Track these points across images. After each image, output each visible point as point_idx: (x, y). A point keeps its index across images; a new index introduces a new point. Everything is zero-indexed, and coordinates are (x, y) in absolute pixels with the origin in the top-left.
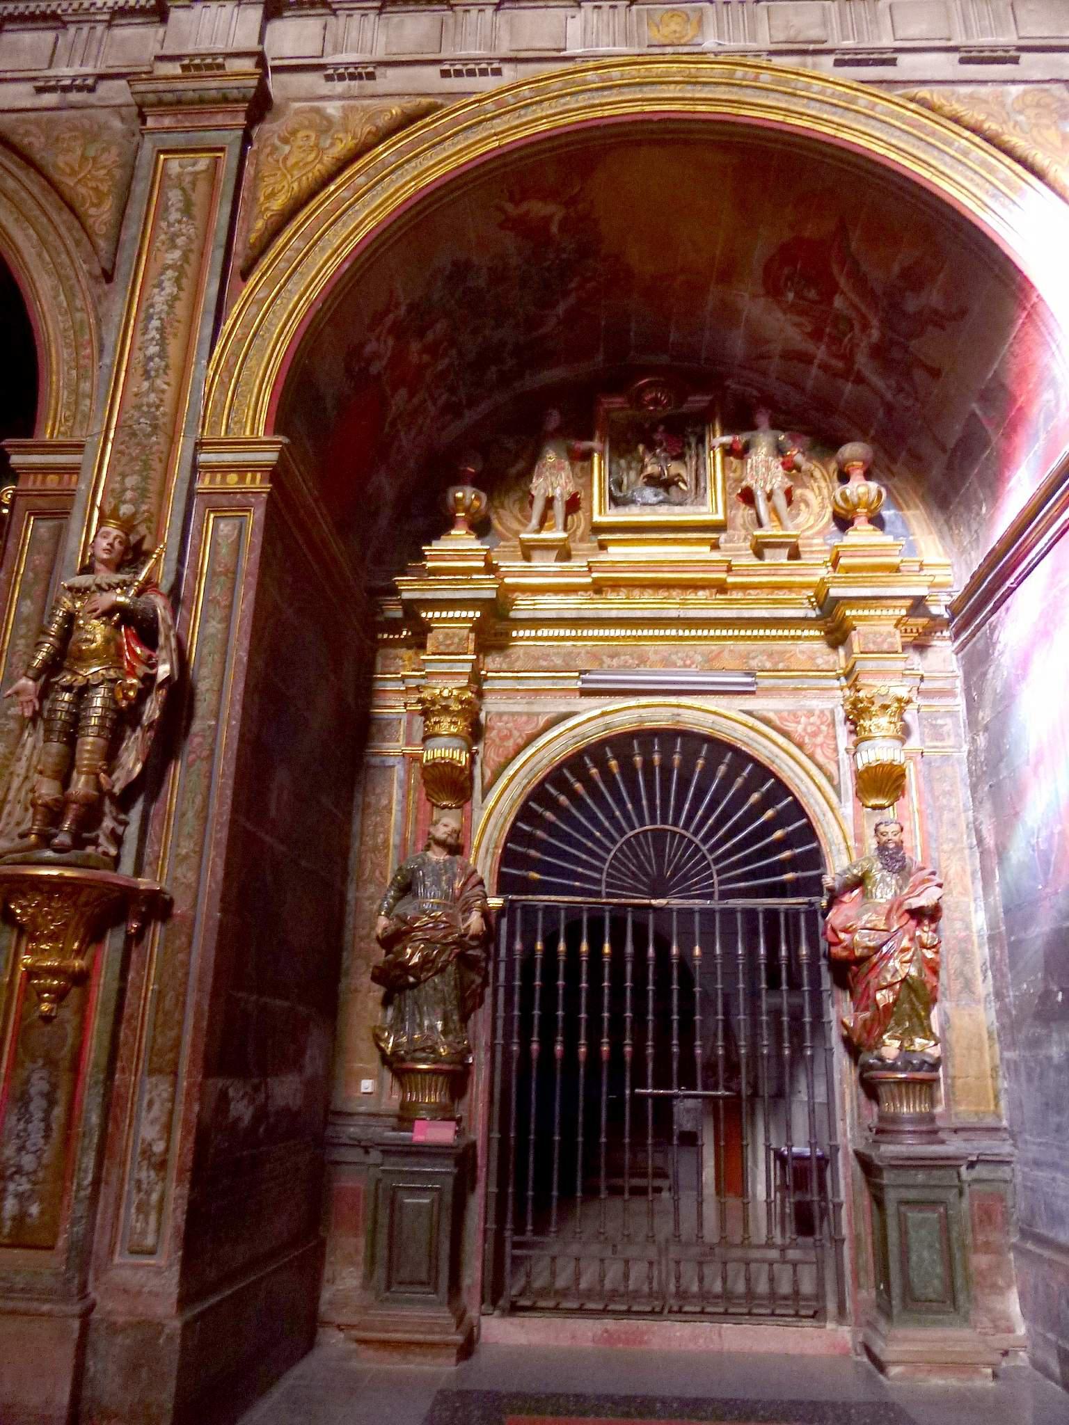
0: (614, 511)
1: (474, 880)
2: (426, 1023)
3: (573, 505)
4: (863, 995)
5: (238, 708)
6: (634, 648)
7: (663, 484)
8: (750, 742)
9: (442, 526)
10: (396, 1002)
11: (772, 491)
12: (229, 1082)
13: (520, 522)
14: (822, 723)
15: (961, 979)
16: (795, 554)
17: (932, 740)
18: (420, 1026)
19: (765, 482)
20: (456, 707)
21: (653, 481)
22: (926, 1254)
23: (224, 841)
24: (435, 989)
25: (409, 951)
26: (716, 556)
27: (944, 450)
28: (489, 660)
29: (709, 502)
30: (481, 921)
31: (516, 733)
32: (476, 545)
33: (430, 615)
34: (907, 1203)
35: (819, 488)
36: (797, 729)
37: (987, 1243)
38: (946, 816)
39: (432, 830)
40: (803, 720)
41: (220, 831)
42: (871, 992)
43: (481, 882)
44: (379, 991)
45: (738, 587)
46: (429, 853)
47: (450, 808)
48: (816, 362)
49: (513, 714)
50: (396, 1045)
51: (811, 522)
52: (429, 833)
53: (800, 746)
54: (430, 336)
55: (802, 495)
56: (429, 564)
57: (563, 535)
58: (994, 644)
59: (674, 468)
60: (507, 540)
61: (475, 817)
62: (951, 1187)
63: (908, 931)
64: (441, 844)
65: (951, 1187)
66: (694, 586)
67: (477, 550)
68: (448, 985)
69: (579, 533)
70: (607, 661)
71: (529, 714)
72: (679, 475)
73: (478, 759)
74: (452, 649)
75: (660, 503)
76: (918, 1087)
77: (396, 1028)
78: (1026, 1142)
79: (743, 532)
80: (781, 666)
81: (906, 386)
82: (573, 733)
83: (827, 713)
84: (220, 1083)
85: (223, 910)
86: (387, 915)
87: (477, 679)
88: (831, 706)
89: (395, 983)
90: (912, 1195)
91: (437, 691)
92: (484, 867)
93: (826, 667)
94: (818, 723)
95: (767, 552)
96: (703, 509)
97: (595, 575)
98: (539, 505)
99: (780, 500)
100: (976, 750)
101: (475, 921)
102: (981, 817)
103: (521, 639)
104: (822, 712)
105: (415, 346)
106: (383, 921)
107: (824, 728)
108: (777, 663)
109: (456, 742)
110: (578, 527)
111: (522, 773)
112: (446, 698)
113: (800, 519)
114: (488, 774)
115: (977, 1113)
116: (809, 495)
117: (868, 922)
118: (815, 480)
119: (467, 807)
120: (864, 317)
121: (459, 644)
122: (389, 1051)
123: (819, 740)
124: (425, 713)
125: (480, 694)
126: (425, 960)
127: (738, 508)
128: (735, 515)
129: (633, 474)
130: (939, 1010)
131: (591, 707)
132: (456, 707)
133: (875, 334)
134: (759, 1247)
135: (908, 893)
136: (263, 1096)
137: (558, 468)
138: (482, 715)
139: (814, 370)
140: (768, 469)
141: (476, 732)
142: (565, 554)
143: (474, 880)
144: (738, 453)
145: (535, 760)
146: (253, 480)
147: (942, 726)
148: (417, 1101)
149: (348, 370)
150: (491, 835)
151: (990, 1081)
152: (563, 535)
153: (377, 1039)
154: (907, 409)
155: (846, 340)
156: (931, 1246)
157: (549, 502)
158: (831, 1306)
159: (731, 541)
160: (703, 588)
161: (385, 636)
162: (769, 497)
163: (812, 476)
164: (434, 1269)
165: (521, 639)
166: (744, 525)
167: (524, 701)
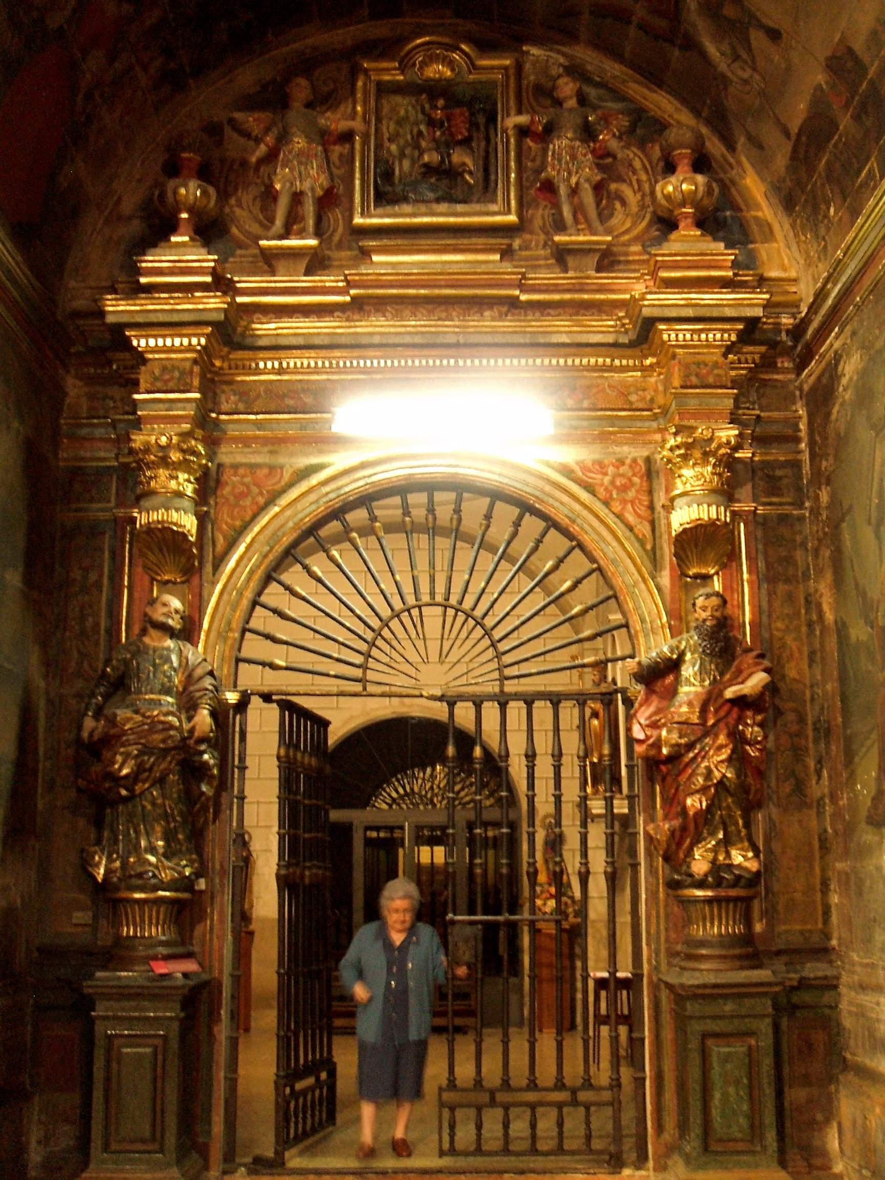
0: (380, 211)
3: (328, 200)
8: (546, 498)
9: (159, 230)
11: (577, 184)
13: (261, 224)
14: (634, 475)
15: (792, 780)
17: (768, 496)
19: (570, 174)
22: (731, 1090)
24: (154, 804)
25: (119, 758)
26: (507, 267)
27: (787, 134)
29: (500, 198)
31: (255, 490)
33: (143, 342)
35: (638, 181)
37: (806, 1076)
39: (148, 610)
40: (611, 470)
42: (681, 795)
46: (146, 640)
47: (175, 583)
48: (635, 20)
49: (253, 467)
50: (108, 871)
51: (628, 224)
52: (146, 615)
55: (617, 190)
58: (839, 378)
60: (247, 247)
62: (764, 1016)
65: (764, 1016)
68: (171, 798)
69: (336, 238)
72: (464, 164)
74: (171, 385)
76: (731, 906)
79: (542, 237)
81: (744, 56)
83: (640, 462)
88: (646, 453)
91: (153, 439)
93: (641, 405)
94: (630, 474)
96: (494, 208)
97: (353, 292)
99: (588, 197)
100: (819, 507)
101: (204, 718)
107: (636, 480)
110: (335, 230)
112: (162, 448)
113: (614, 221)
115: (802, 933)
116: (627, 192)
118: (634, 172)
119: (195, 581)
121: (179, 379)
122: (100, 878)
123: (631, 494)
127: (537, 207)
128: (533, 215)
134: (520, 1090)
137: (304, 157)
139: (632, 31)
147: (780, 478)
148: (135, 936)
151: (819, 896)
152: (313, 242)
154: (746, 82)
156: (737, 1082)
157: (297, 198)
159: (527, 248)
162: (574, 191)
163: (631, 165)
166: (543, 228)
167: (266, 449)
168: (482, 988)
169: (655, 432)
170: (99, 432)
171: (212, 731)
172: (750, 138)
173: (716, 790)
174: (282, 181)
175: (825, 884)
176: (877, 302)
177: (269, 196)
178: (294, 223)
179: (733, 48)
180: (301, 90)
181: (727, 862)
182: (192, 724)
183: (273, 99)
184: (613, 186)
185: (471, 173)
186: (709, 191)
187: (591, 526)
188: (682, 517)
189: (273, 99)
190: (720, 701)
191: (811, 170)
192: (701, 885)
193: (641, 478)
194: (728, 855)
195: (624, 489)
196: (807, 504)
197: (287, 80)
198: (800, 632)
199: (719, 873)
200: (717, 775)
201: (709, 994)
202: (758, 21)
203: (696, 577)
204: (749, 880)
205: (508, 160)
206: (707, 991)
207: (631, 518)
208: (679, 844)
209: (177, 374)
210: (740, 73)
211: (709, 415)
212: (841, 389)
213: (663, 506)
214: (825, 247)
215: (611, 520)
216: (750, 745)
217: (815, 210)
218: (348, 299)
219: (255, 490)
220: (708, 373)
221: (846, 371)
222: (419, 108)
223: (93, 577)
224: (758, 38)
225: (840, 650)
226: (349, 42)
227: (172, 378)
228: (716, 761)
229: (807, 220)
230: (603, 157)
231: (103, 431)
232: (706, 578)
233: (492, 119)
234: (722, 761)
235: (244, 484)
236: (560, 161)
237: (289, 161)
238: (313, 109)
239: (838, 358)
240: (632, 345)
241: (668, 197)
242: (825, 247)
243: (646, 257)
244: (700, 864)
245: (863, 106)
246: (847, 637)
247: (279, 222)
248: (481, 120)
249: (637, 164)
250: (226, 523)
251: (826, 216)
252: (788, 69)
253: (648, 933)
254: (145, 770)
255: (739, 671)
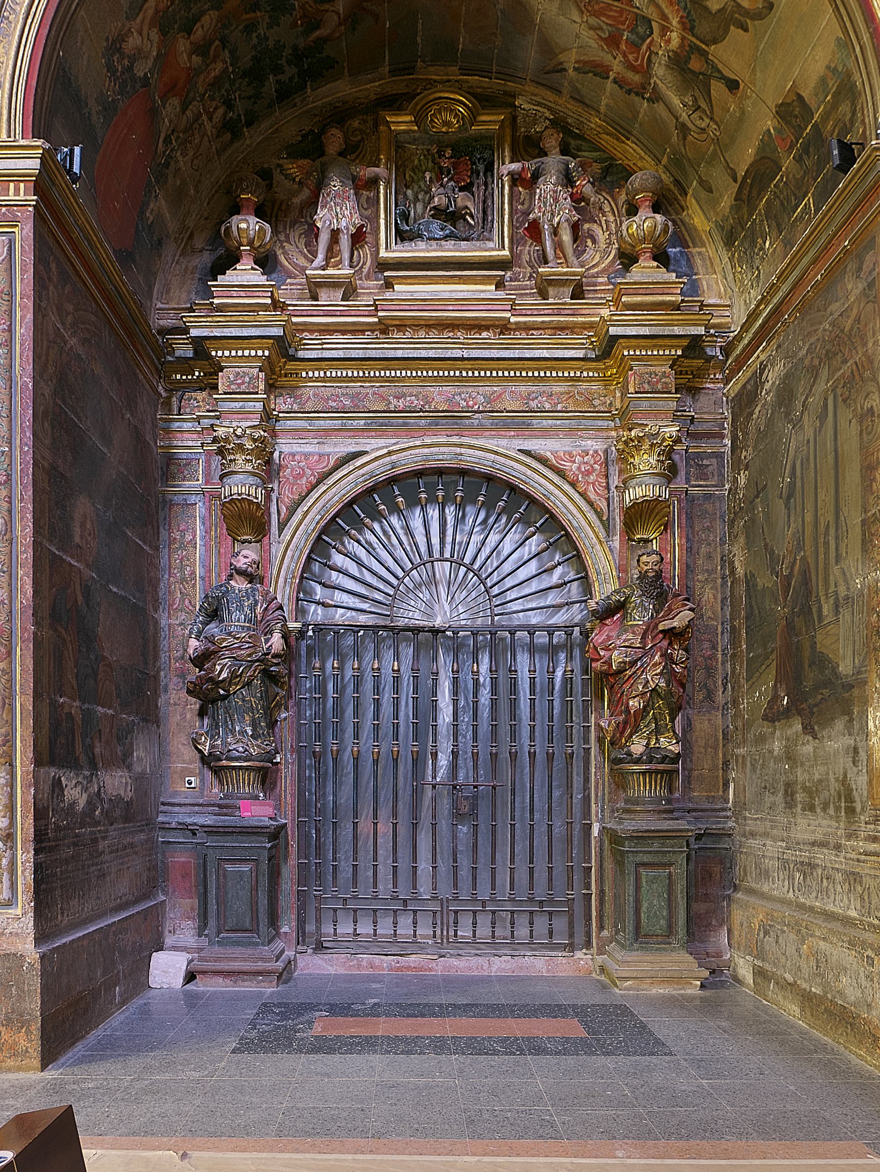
0: (400, 247)
1: (273, 605)
2: (237, 729)
3: (358, 238)
4: (618, 702)
5: (29, 434)
6: (420, 389)
7: (451, 217)
9: (230, 260)
10: (210, 712)
11: (558, 223)
12: (61, 772)
16: (578, 293)
18: (233, 731)
20: (249, 445)
21: (439, 213)
23: (30, 561)
24: (243, 701)
25: (218, 668)
26: (501, 294)
28: (280, 400)
29: (496, 238)
30: (282, 641)
31: (309, 472)
32: (262, 280)
34: (644, 865)
36: (571, 468)
38: (704, 549)
40: (578, 459)
41: (25, 552)
43: (281, 608)
44: (195, 704)
45: (520, 327)
47: (250, 543)
49: (306, 455)
50: (212, 747)
53: (573, 485)
54: (199, 33)
56: (216, 301)
57: (348, 271)
59: (462, 199)
61: (273, 550)
63: (661, 648)
64: (241, 573)
66: (477, 326)
67: (263, 286)
68: (256, 697)
69: (365, 270)
70: (394, 402)
71: (321, 455)
72: (467, 207)
73: (274, 496)
74: (243, 388)
75: (446, 238)
77: (213, 732)
78: (745, 818)
80: (559, 408)
81: (703, 105)
82: (362, 471)
84: (52, 771)
85: (36, 623)
86: (197, 638)
87: (268, 417)
89: (209, 697)
90: (646, 859)
92: (283, 596)
95: (551, 291)
96: (491, 245)
98: (324, 238)
99: (566, 237)
101: (276, 641)
102: (735, 550)
103: (311, 380)
104: (596, 452)
105: (182, 45)
106: (193, 643)
108: (556, 404)
109: (251, 480)
110: (364, 264)
111: (315, 510)
112: (239, 437)
113: (585, 256)
114: (284, 510)
117: (625, 641)
119: (266, 540)
120: (664, 17)
123: (592, 478)
124: (221, 452)
125: (274, 434)
126: (233, 675)
127: (524, 245)
129: (420, 207)
130: (683, 716)
131: (375, 445)
132: (249, 445)
133: (675, 38)
135: (663, 617)
136: (96, 786)
138: (276, 455)
140: (556, 200)
141: (268, 469)
142: (350, 291)
143: (273, 605)
144: (525, 182)
145: (326, 497)
146: (17, 192)
147: (707, 466)
149: (110, 67)
150: (288, 567)
152: (348, 271)
153: (195, 742)
155: (644, 47)
157: (335, 235)
158: (580, 938)
160: (487, 328)
161: (178, 377)
162: (555, 232)
163: (601, 209)
164: (255, 918)
165: (311, 380)
166: (529, 263)
168: (650, 772)
169: (611, 430)
170: (187, 426)
171: (283, 650)
172: (701, 182)
173: (651, 695)
174: (323, 218)
175: (726, 763)
176: (803, 319)
177: (313, 232)
178: (332, 258)
179: (695, 100)
180: (335, 140)
181: (657, 745)
182: (269, 644)
183: (311, 148)
184: (586, 226)
185: (472, 217)
186: (665, 230)
187: (561, 502)
188: (637, 493)
189: (311, 148)
190: (656, 631)
191: (752, 209)
192: (638, 761)
193: (601, 465)
194: (657, 740)
195: (588, 473)
196: (727, 487)
197: (323, 131)
198: (716, 582)
199: (650, 754)
200: (652, 685)
201: (640, 837)
202: (719, 71)
203: (640, 540)
204: (672, 759)
205: (503, 203)
206: (640, 834)
207: (592, 496)
208: (622, 733)
209: (247, 379)
210: (698, 123)
211: (655, 414)
212: (764, 392)
213: (616, 487)
214: (758, 276)
215: (576, 497)
216: (676, 664)
217: (753, 243)
218: (376, 320)
219: (309, 472)
220: (657, 382)
221: (769, 378)
222: (430, 157)
223: (189, 537)
224: (717, 88)
225: (749, 597)
226: (373, 97)
227: (243, 383)
228: (652, 676)
229: (745, 253)
230: (578, 200)
231: (190, 424)
232: (647, 541)
233: (489, 168)
234: (656, 675)
235: (300, 468)
236: (545, 205)
237: (327, 202)
238: (345, 157)
239: (763, 367)
240: (597, 359)
241: (631, 236)
242: (758, 276)
243: (611, 287)
244: (637, 747)
245: (806, 150)
246: (755, 585)
247: (321, 256)
248: (481, 167)
249: (607, 209)
250: (288, 497)
251: (762, 249)
252: (741, 119)
253: (597, 795)
254: (237, 677)
255: (670, 610)
